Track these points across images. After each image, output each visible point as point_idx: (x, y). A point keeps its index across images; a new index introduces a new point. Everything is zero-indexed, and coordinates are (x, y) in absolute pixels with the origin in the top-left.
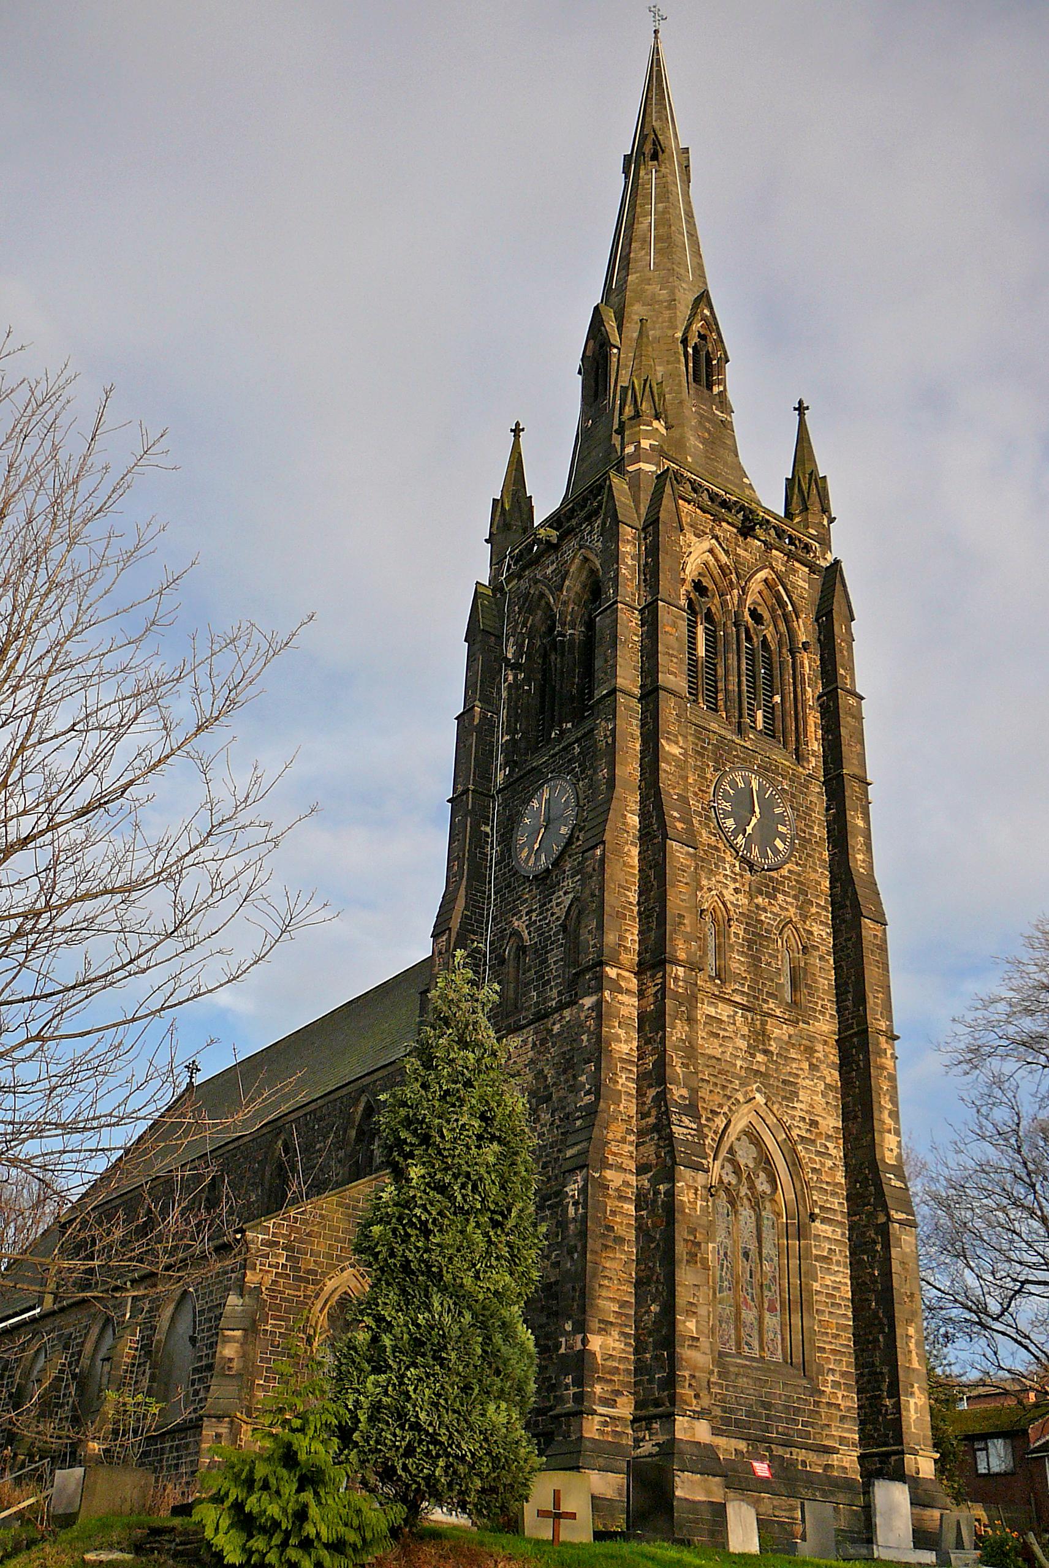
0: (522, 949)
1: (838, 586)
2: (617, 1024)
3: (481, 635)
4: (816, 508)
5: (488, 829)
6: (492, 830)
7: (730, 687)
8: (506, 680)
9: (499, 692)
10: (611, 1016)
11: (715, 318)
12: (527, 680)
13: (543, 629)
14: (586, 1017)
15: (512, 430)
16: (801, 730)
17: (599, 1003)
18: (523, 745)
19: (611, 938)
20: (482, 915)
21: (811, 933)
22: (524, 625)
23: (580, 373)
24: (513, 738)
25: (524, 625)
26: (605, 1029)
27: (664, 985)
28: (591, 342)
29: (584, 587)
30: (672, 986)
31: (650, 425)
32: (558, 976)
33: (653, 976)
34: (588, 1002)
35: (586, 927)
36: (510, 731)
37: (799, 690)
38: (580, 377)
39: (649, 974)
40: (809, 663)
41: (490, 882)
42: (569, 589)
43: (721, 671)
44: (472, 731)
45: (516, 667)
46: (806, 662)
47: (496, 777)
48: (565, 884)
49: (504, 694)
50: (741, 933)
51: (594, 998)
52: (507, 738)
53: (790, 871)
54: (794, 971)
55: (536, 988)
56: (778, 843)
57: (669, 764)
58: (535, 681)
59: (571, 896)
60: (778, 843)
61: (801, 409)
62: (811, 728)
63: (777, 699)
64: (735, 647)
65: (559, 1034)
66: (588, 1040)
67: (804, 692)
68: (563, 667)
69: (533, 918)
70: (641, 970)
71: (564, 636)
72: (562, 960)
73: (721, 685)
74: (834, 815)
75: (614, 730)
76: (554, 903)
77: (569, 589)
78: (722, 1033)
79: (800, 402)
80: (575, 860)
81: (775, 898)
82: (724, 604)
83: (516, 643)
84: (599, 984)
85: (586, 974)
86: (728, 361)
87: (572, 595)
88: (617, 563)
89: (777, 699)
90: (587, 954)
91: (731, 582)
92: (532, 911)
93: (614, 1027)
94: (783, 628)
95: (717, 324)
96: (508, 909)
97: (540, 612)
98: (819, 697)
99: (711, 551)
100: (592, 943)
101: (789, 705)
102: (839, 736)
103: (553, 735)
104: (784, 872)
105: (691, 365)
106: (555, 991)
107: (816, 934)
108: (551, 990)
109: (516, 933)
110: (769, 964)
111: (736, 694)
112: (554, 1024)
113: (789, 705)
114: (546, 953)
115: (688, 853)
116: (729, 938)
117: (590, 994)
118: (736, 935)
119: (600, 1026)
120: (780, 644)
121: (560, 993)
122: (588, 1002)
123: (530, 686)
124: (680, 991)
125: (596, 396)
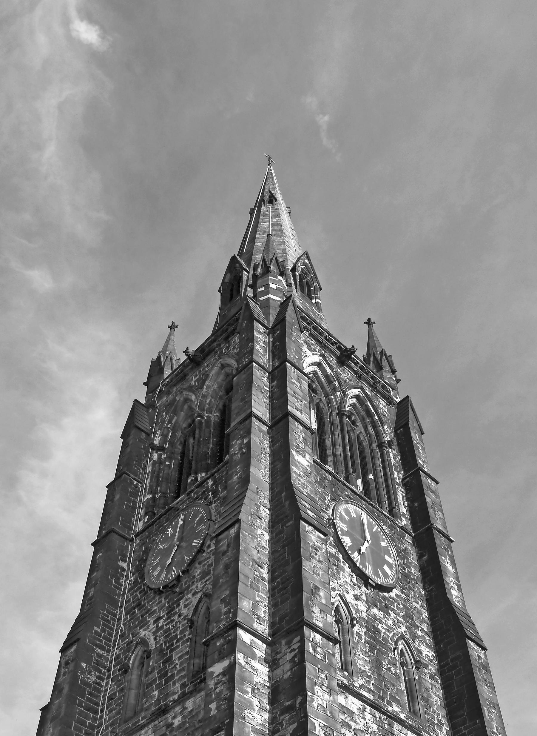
0: (148, 654)
1: (410, 411)
2: (250, 690)
3: (134, 430)
4: (387, 368)
5: (125, 565)
6: (128, 565)
7: (338, 453)
8: (151, 459)
9: (145, 469)
10: (244, 680)
11: (312, 266)
12: (169, 458)
13: (184, 425)
14: (216, 684)
15: (169, 327)
16: (393, 496)
17: (232, 667)
18: (162, 501)
19: (245, 604)
20: (111, 635)
21: (421, 653)
22: (170, 422)
23: (219, 291)
24: (154, 498)
25: (170, 422)
26: (237, 693)
27: (302, 650)
28: (229, 275)
29: (220, 387)
30: (311, 651)
31: (277, 277)
32: (183, 669)
33: (289, 643)
34: (218, 668)
35: (219, 597)
36: (153, 492)
37: (388, 471)
38: (219, 295)
39: (283, 642)
40: (393, 456)
41: (121, 606)
42: (208, 387)
43: (329, 443)
44: (119, 490)
45: (160, 449)
46: (391, 455)
47: (136, 524)
48: (194, 587)
49: (149, 469)
50: (363, 634)
51: (225, 663)
52: (149, 496)
53: (396, 595)
54: (409, 683)
55: (158, 687)
56: (386, 567)
57: (298, 469)
58: (175, 459)
59: (199, 596)
60: (386, 567)
61: (369, 323)
62: (400, 498)
63: (371, 476)
64: (339, 428)
65: (180, 727)
66: (218, 708)
67: (392, 473)
68: (200, 437)
69: (161, 624)
70: (272, 642)
71: (202, 417)
72: (187, 653)
73: (329, 452)
74: (427, 561)
75: (249, 443)
76: (182, 605)
77: (208, 387)
78: (354, 725)
79: (369, 320)
80: (205, 565)
81: (388, 613)
82: (329, 401)
83: (162, 434)
84: (231, 647)
85: (218, 638)
86: (321, 289)
87: (210, 391)
88: (253, 342)
89: (371, 476)
90: (219, 621)
91: (335, 387)
92: (159, 618)
93: (247, 692)
94: (371, 431)
95: (313, 269)
96: (138, 613)
97: (182, 414)
98: (403, 480)
99: (319, 364)
100: (223, 611)
101: (381, 480)
102: (424, 502)
103: (189, 481)
104: (393, 594)
105: (298, 280)
106: (178, 685)
107: (424, 653)
108: (174, 684)
109: (144, 642)
110: (389, 669)
111: (342, 458)
112: (174, 717)
113: (381, 480)
114: (172, 650)
115: (319, 537)
116: (353, 637)
117: (221, 659)
118: (359, 635)
119: (232, 690)
120: (370, 442)
121: (184, 686)
122: (218, 668)
123: (171, 463)
124: (319, 657)
125: (231, 298)
